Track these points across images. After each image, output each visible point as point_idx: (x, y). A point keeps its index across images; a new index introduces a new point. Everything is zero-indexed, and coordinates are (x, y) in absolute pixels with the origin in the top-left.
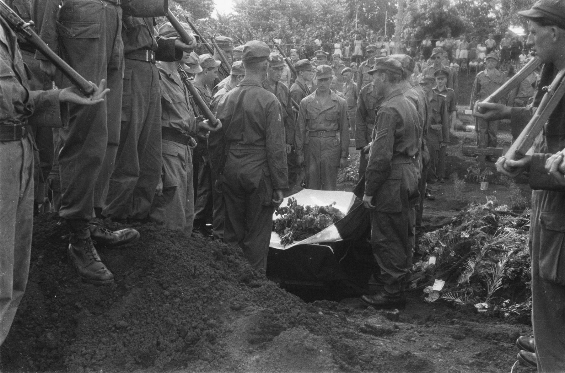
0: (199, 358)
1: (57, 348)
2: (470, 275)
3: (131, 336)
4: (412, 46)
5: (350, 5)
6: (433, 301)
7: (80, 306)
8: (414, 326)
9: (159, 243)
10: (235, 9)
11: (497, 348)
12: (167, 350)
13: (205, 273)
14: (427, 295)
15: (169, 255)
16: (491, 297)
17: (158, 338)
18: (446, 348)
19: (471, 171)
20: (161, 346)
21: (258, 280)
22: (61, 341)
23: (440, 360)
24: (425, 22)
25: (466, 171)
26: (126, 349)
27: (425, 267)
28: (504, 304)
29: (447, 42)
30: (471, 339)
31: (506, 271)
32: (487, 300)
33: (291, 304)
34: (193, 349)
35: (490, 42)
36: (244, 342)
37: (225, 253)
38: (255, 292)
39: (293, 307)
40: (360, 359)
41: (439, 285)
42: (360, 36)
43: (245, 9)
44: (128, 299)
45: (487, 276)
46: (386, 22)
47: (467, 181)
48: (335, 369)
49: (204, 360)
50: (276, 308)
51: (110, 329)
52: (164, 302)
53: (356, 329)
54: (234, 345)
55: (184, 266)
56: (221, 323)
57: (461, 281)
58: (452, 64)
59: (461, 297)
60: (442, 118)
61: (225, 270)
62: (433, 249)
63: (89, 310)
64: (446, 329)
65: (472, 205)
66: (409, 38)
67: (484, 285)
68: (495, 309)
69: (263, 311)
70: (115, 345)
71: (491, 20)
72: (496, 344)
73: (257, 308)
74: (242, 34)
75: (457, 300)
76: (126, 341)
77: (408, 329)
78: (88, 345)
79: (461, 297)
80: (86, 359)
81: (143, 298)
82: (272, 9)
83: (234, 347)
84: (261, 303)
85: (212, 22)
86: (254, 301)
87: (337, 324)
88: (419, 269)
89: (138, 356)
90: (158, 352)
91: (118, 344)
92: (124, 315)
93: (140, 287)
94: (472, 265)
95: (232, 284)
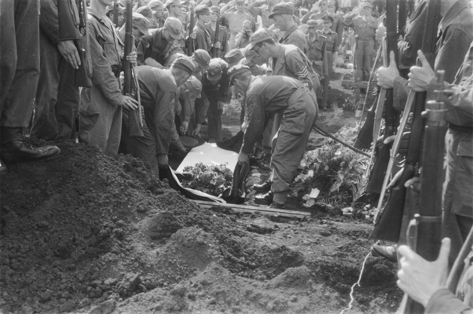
0: (109, 252)
2: (339, 185)
6: (309, 206)
7: (8, 209)
8: (291, 225)
11: (355, 243)
13: (116, 182)
14: (305, 202)
15: (86, 166)
16: (355, 203)
17: (74, 235)
18: (315, 243)
19: (348, 102)
21: (162, 188)
23: (309, 252)
25: (344, 101)
26: (46, 244)
27: (305, 179)
28: (365, 208)
32: (352, 206)
33: (189, 208)
34: (103, 244)
38: (159, 198)
39: (191, 210)
41: (315, 193)
44: (49, 203)
45: (353, 186)
47: (345, 109)
49: (112, 253)
51: (33, 227)
52: (80, 205)
53: (243, 228)
54: (138, 241)
56: (129, 223)
57: (333, 190)
59: (332, 203)
60: (323, 55)
61: (134, 180)
62: (312, 164)
63: (16, 212)
64: (316, 228)
67: (350, 193)
68: (358, 212)
69: (163, 213)
72: (354, 239)
76: (46, 237)
77: (286, 228)
78: (14, 241)
79: (332, 203)
80: (12, 253)
81: (62, 202)
84: (163, 207)
86: (158, 205)
87: (228, 224)
89: (56, 250)
90: (74, 246)
94: (341, 177)
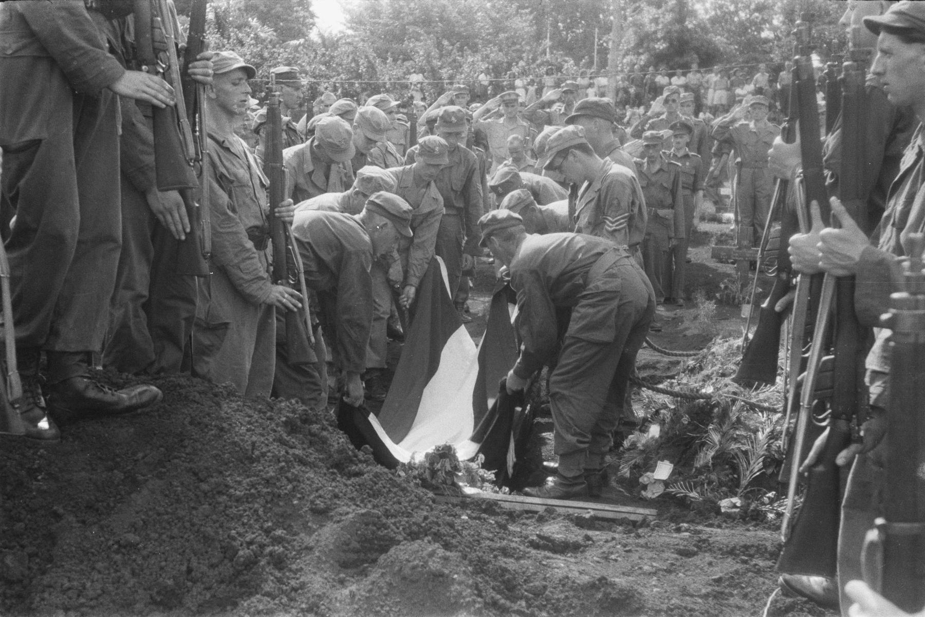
0: (257, 593)
1: (21, 581)
2: (712, 453)
3: (144, 558)
5: (535, 18)
6: (654, 497)
7: (61, 511)
8: (617, 536)
9: (195, 406)
10: (349, 25)
12: (204, 580)
13: (269, 454)
14: (645, 487)
16: (746, 488)
17: (189, 560)
18: (665, 570)
19: (726, 288)
20: (193, 574)
22: (29, 568)
23: (655, 590)
24: (656, 46)
25: (718, 287)
27: (643, 441)
28: (766, 500)
29: (693, 78)
30: (707, 554)
31: (769, 446)
35: (761, 78)
36: (332, 565)
38: (353, 485)
39: (417, 507)
40: (526, 591)
41: (664, 470)
42: (552, 69)
43: (365, 25)
44: (140, 499)
46: (596, 47)
47: (720, 302)
48: (477, 606)
50: (387, 510)
53: (522, 542)
55: (234, 443)
56: (294, 535)
57: (700, 462)
58: (701, 115)
59: (699, 489)
61: (304, 449)
65: (719, 341)
67: (735, 469)
69: (363, 515)
70: (119, 574)
71: (766, 41)
73: (354, 510)
74: (358, 65)
75: (691, 495)
77: (607, 541)
78: (74, 575)
81: (166, 496)
82: (409, 24)
83: (315, 573)
84: (362, 501)
85: (309, 46)
86: (352, 499)
87: (491, 535)
88: (633, 446)
90: (189, 584)
91: (123, 571)
92: (133, 525)
93: (161, 478)
95: (315, 472)
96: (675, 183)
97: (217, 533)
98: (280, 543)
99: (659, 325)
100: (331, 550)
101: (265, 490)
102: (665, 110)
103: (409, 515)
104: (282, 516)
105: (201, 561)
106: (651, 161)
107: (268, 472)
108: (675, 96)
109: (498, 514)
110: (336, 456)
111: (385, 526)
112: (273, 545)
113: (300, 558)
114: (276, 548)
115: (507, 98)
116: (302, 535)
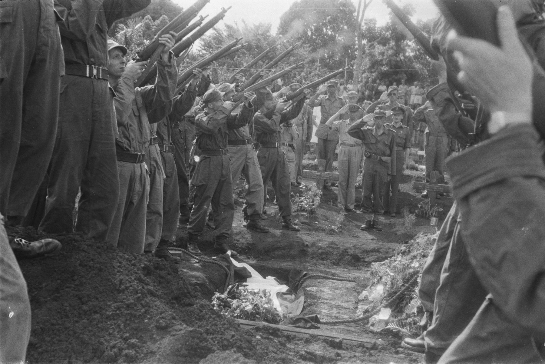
4: (369, 90)
8: (357, 354)
9: (84, 254)
13: (131, 288)
15: (93, 266)
19: (421, 207)
29: (402, 88)
37: (156, 268)
39: (228, 329)
50: (208, 330)
56: (144, 343)
61: (155, 286)
66: (367, 82)
69: (191, 331)
77: (350, 358)
81: (59, 312)
87: (275, 350)
93: (56, 301)
96: (392, 142)
97: (90, 339)
98: (133, 348)
99: (381, 227)
100: (168, 354)
101: (126, 312)
102: (389, 99)
103: (223, 334)
104: (136, 329)
105: (78, 358)
106: (378, 128)
107: (129, 300)
108: (395, 92)
109: (279, 337)
110: (176, 292)
111: (206, 340)
112: (129, 349)
113: (146, 359)
114: (130, 351)
115: (294, 87)
116: (149, 343)
